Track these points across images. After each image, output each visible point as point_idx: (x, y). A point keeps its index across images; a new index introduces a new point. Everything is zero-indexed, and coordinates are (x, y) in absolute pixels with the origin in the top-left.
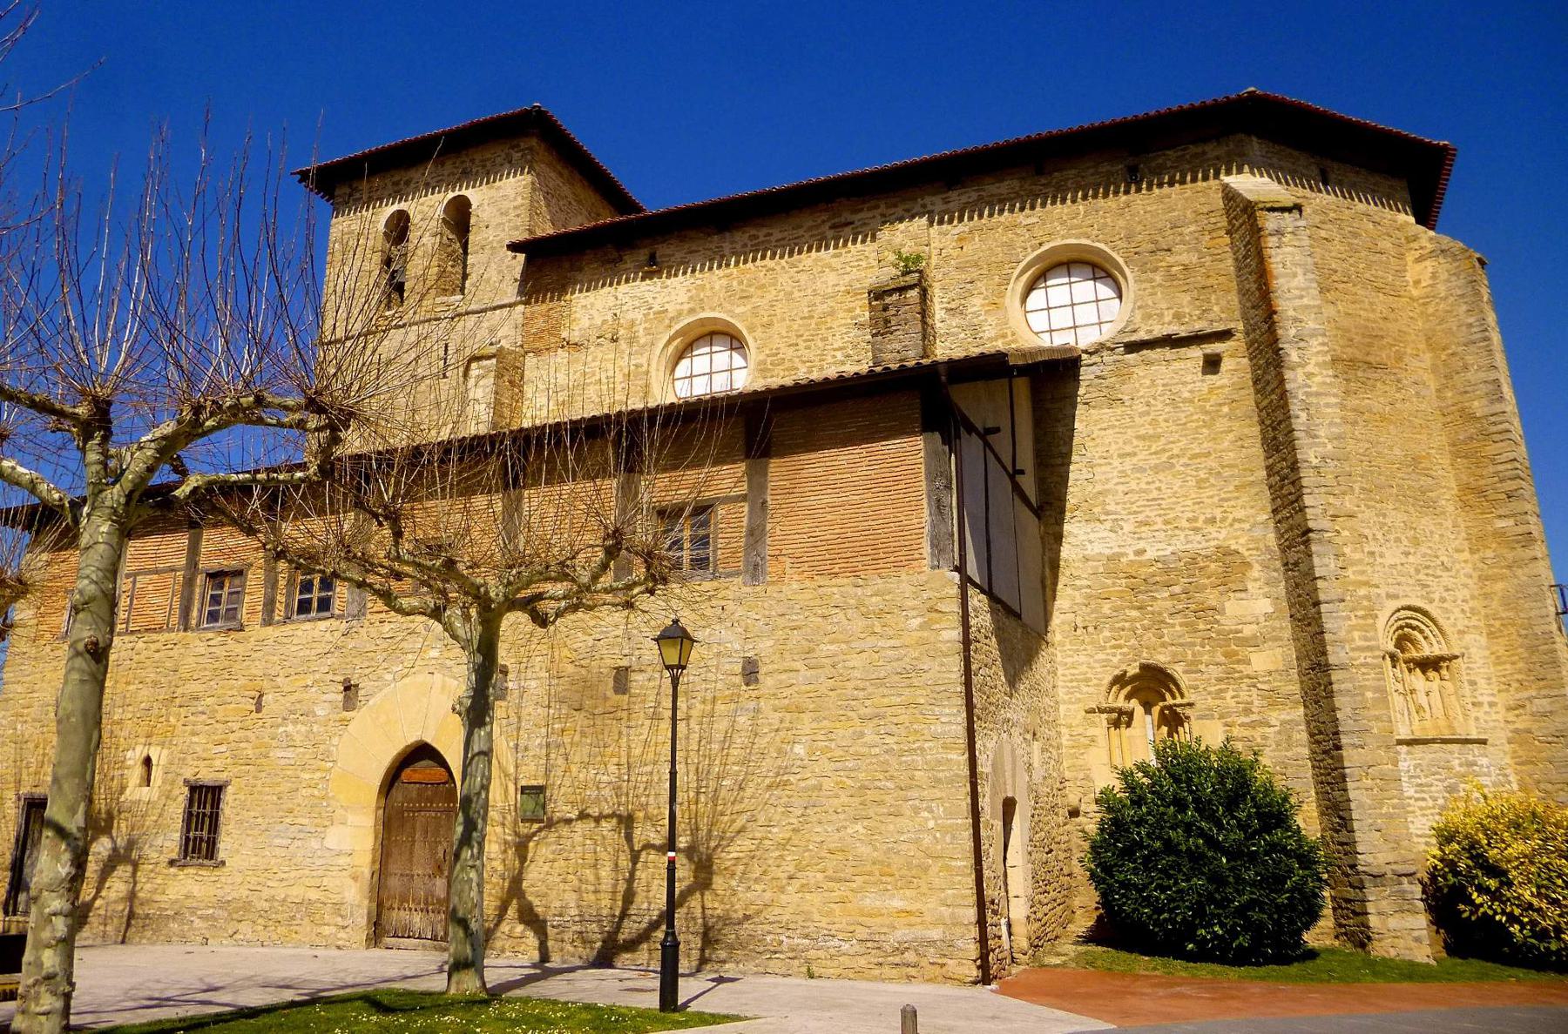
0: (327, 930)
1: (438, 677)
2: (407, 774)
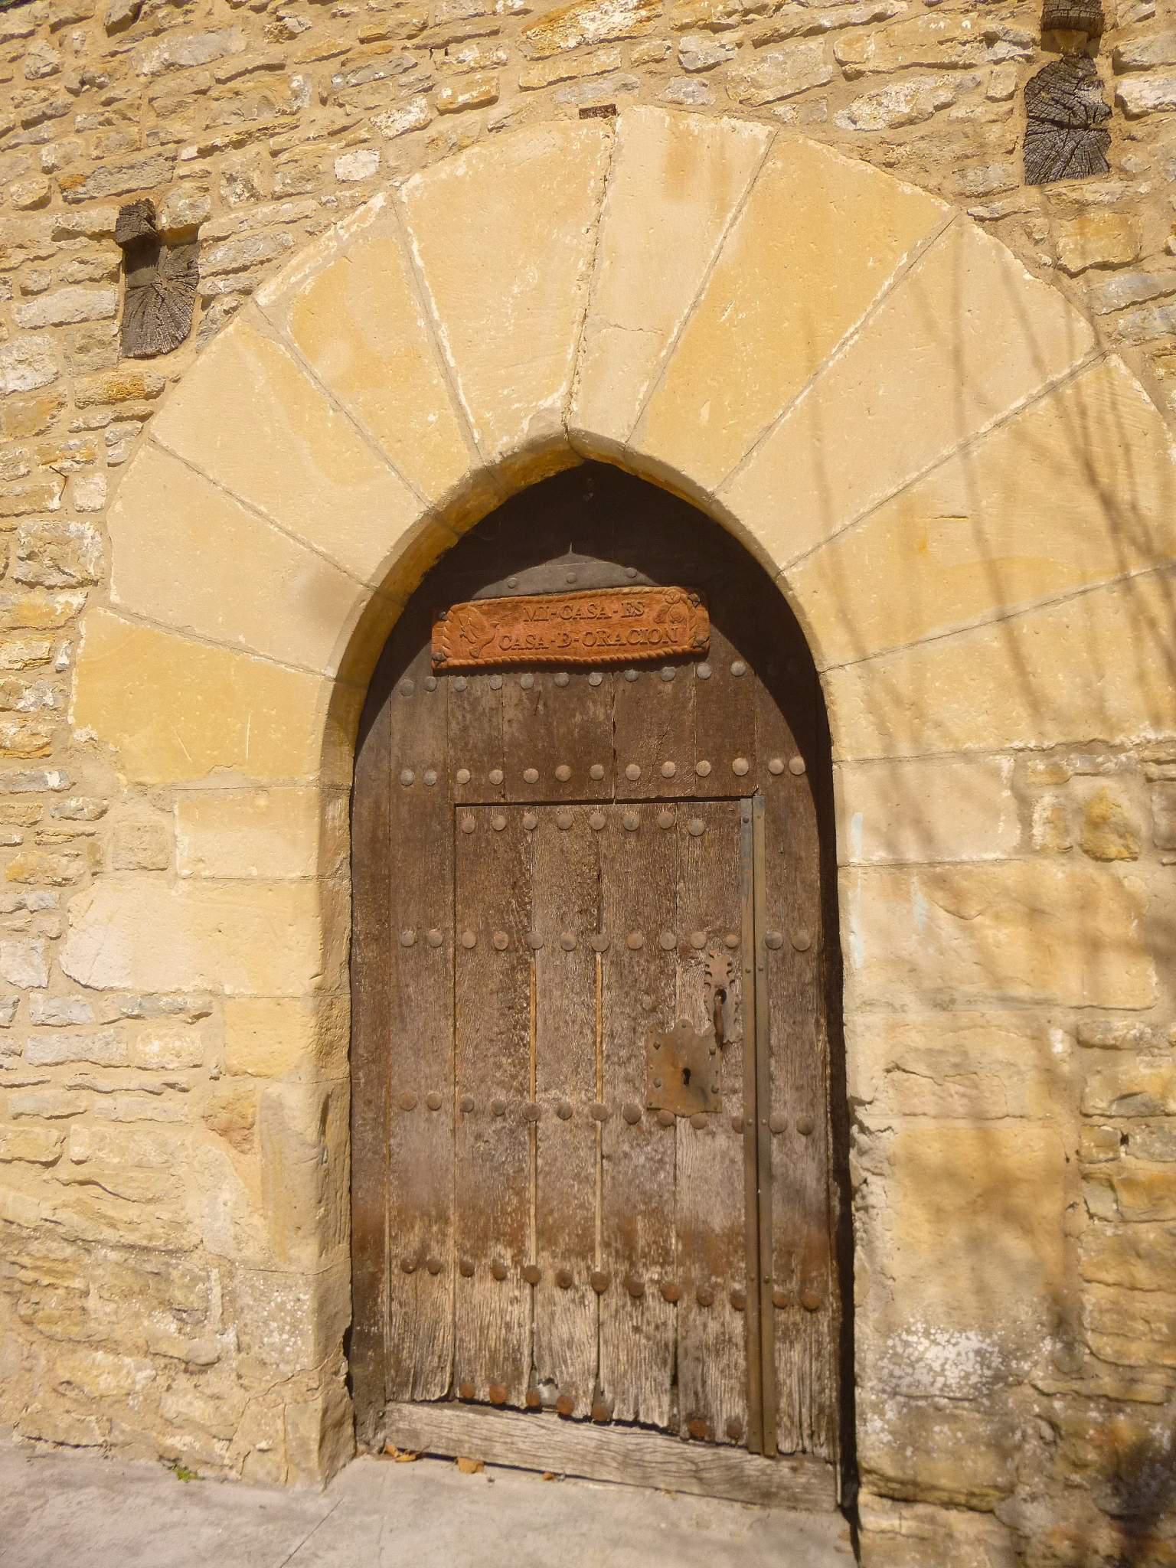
0: (104, 1373)
1: (643, 124)
2: (464, 630)
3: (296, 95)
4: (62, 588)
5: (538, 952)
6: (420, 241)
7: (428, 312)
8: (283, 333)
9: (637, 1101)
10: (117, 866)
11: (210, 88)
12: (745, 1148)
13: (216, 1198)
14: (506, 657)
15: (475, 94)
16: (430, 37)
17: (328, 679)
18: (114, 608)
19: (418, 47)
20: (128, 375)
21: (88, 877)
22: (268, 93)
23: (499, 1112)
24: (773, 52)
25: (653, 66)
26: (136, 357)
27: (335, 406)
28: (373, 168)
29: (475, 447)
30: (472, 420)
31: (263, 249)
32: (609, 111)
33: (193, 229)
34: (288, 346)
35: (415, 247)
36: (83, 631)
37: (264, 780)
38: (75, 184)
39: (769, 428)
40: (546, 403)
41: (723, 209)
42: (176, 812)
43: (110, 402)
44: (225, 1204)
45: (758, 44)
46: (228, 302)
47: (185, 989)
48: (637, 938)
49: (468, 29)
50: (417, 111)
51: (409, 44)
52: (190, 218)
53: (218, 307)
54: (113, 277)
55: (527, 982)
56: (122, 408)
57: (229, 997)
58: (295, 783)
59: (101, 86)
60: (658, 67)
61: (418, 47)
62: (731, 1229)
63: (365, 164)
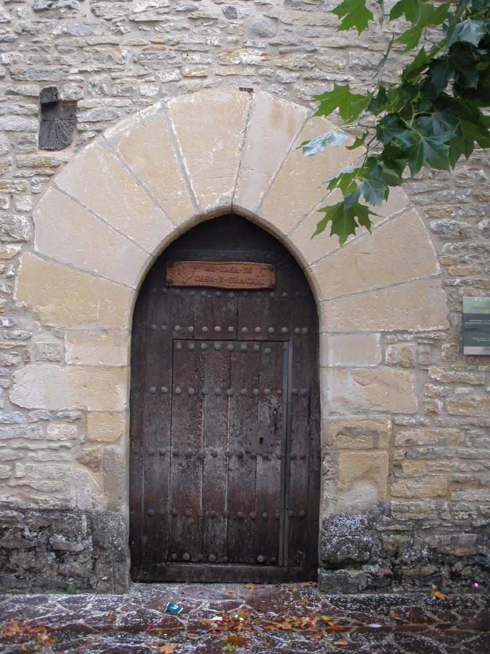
3: (124, 58)
4: (9, 242)
5: (206, 396)
6: (175, 124)
7: (178, 152)
8: (116, 151)
9: (242, 450)
10: (37, 359)
11: (84, 47)
12: (281, 465)
13: (84, 489)
14: (197, 284)
15: (199, 73)
16: (181, 47)
17: (134, 289)
18: (36, 253)
19: (176, 50)
20: (43, 157)
21: (22, 363)
22: (111, 54)
23: (189, 456)
24: (310, 84)
25: (266, 78)
26: (45, 149)
27: (138, 183)
28: (156, 93)
29: (197, 206)
30: (196, 196)
31: (108, 116)
32: (250, 91)
33: (75, 102)
34: (118, 156)
35: (173, 126)
36: (21, 262)
37: (106, 327)
38: (19, 73)
39: (306, 215)
40: (225, 194)
41: (292, 135)
42: (66, 339)
43: (34, 167)
44: (88, 491)
45: (307, 79)
46: (91, 134)
47: (69, 408)
48: (244, 391)
49: (196, 48)
50: (175, 75)
51: (172, 48)
52: (74, 97)
53: (85, 136)
54: (36, 115)
55: (201, 407)
56: (40, 171)
57: (90, 412)
58: (119, 329)
59: (32, 35)
60: (269, 79)
61: (176, 50)
62: (275, 492)
63: (153, 91)
